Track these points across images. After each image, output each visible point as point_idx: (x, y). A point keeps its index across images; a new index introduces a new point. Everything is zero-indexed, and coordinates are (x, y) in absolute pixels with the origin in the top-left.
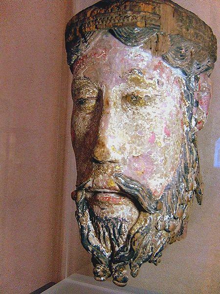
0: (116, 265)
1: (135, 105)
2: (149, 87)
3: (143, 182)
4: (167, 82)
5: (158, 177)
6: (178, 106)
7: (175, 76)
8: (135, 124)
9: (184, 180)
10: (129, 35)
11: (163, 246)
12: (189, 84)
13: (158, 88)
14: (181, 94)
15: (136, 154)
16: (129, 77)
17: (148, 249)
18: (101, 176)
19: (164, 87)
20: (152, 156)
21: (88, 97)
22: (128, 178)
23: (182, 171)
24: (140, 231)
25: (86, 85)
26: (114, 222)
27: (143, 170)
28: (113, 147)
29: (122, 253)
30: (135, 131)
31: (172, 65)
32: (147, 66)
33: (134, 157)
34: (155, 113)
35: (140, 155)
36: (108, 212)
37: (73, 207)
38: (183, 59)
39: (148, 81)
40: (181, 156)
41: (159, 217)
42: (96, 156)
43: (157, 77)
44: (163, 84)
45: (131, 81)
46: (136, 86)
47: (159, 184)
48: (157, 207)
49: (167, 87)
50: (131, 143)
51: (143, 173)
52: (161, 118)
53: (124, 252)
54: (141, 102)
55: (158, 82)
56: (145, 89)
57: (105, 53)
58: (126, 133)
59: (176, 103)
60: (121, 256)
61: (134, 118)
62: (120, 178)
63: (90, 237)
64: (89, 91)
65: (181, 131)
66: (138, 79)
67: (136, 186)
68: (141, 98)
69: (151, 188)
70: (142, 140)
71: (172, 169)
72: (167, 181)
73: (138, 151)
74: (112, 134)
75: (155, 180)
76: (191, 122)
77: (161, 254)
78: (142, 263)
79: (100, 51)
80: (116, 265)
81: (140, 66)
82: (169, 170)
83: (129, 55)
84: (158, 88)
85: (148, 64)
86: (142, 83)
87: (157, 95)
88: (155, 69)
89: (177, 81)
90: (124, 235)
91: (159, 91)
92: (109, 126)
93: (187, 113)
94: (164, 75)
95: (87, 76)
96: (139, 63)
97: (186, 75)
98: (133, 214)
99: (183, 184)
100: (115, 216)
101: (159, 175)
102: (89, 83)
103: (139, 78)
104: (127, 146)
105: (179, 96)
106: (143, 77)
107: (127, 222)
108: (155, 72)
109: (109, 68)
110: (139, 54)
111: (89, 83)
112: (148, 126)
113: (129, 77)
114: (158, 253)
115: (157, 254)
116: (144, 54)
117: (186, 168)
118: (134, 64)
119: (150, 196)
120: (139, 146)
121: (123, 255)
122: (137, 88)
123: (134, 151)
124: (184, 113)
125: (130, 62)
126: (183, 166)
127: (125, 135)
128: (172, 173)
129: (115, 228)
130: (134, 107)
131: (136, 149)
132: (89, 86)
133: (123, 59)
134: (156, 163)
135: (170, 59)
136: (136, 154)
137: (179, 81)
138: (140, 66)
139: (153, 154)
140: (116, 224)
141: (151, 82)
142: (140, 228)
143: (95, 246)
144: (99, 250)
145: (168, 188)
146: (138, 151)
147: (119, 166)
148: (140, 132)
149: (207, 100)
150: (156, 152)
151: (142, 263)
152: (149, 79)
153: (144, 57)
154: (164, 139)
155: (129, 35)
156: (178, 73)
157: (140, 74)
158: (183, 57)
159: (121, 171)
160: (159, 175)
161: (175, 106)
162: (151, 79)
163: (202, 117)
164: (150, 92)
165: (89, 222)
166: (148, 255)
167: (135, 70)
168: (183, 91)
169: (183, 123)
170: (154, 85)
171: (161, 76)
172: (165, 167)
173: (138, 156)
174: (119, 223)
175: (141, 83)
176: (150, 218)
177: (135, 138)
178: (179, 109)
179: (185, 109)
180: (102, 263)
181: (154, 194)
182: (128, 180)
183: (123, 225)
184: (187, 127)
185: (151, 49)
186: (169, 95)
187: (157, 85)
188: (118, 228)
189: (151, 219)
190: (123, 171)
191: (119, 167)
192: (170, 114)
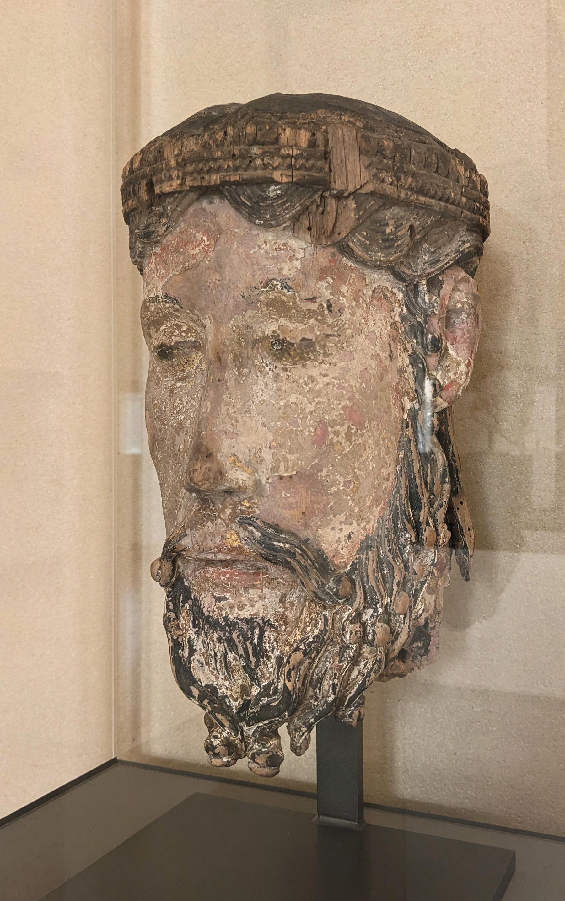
0: (254, 728)
1: (280, 359)
2: (309, 318)
3: (304, 534)
4: (354, 303)
5: (341, 523)
6: (384, 355)
7: (375, 285)
8: (282, 403)
9: (408, 526)
10: (257, 203)
11: (364, 681)
12: (416, 298)
13: (330, 320)
14: (393, 325)
15: (286, 471)
16: (262, 298)
17: (326, 688)
18: (209, 524)
19: (346, 315)
20: (323, 474)
21: (177, 343)
22: (271, 527)
23: (401, 504)
24: (302, 647)
25: (169, 313)
26: (245, 627)
27: (304, 506)
28: (233, 458)
29: (265, 700)
30: (283, 418)
31: (363, 263)
32: (304, 272)
33: (281, 478)
34: (326, 375)
35: (294, 473)
36: (231, 607)
37: (341, 91)
38: (390, 247)
39: (306, 306)
40: (398, 469)
41: (347, 613)
42: (195, 480)
43: (328, 294)
44: (341, 311)
45: (268, 305)
46: (280, 317)
47: (343, 538)
48: (337, 590)
49: (353, 314)
50: (275, 448)
51: (304, 513)
52: (340, 387)
53: (269, 696)
54: (292, 353)
55: (329, 306)
56: (301, 322)
57: (207, 243)
58: (264, 425)
59: (378, 348)
60: (262, 707)
61: (279, 389)
62: (251, 528)
63: (195, 665)
64: (179, 327)
65: (396, 412)
66: (283, 302)
67: (287, 546)
68: (293, 344)
69: (324, 546)
70: (300, 438)
71: (376, 502)
72: (364, 528)
73: (290, 464)
74: (229, 428)
75: (333, 529)
76: (423, 388)
77: (363, 698)
78: (312, 720)
79: (199, 236)
80: (254, 728)
81: (285, 272)
82: (368, 504)
83: (259, 247)
84: (330, 320)
85: (303, 267)
86: (294, 311)
87: (328, 336)
88: (321, 278)
89: (380, 295)
90: (269, 658)
91: (331, 326)
92: (223, 409)
93: (410, 369)
94: (344, 289)
95: (172, 295)
96: (283, 265)
97: (404, 280)
98: (286, 609)
99: (407, 535)
100: (245, 614)
101: (342, 517)
102: (177, 310)
103: (284, 298)
104: (267, 455)
105: (387, 331)
106: (294, 298)
107: (273, 626)
108: (322, 284)
109: (218, 277)
110: (284, 245)
111: (177, 310)
112: (311, 408)
113: (262, 298)
114: (354, 697)
115: (351, 700)
116: (294, 243)
117: (414, 499)
118: (273, 268)
119: (322, 565)
120: (291, 452)
121: (268, 704)
122: (283, 321)
123: (282, 465)
124: (402, 371)
125: (264, 262)
126: (403, 492)
127: (260, 427)
128: (376, 510)
129: (248, 643)
130: (280, 365)
131: (286, 460)
132: (178, 317)
133: (247, 255)
134: (334, 489)
135: (358, 250)
136: (286, 471)
137: (385, 296)
138: (285, 272)
139: (325, 470)
140: (249, 633)
141: (314, 307)
142: (301, 641)
143: (207, 686)
144: (217, 696)
145: (366, 546)
146: (290, 464)
147: (250, 499)
148: (294, 422)
149: (468, 331)
150: (332, 466)
151: (312, 720)
152: (308, 299)
153: (294, 251)
154: (349, 436)
155: (257, 203)
156: (382, 280)
157: (285, 291)
158: (389, 243)
159: (254, 512)
160: (342, 517)
161: (375, 356)
162: (313, 300)
163: (455, 374)
164: (312, 329)
165: (191, 632)
166: (326, 702)
167: (275, 282)
168: (397, 319)
169: (400, 394)
170: (322, 313)
171: (336, 291)
172: (356, 497)
173: (291, 477)
174: (257, 631)
175: (290, 309)
176: (325, 616)
177: (283, 435)
178: (387, 362)
179: (404, 360)
180: (223, 726)
181: (332, 562)
182: (270, 531)
183: (266, 634)
184: (412, 400)
185: (309, 229)
186: (359, 332)
187: (326, 312)
188: (255, 641)
189: (326, 619)
190: (258, 512)
191: (249, 502)
192: (362, 377)
